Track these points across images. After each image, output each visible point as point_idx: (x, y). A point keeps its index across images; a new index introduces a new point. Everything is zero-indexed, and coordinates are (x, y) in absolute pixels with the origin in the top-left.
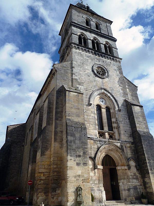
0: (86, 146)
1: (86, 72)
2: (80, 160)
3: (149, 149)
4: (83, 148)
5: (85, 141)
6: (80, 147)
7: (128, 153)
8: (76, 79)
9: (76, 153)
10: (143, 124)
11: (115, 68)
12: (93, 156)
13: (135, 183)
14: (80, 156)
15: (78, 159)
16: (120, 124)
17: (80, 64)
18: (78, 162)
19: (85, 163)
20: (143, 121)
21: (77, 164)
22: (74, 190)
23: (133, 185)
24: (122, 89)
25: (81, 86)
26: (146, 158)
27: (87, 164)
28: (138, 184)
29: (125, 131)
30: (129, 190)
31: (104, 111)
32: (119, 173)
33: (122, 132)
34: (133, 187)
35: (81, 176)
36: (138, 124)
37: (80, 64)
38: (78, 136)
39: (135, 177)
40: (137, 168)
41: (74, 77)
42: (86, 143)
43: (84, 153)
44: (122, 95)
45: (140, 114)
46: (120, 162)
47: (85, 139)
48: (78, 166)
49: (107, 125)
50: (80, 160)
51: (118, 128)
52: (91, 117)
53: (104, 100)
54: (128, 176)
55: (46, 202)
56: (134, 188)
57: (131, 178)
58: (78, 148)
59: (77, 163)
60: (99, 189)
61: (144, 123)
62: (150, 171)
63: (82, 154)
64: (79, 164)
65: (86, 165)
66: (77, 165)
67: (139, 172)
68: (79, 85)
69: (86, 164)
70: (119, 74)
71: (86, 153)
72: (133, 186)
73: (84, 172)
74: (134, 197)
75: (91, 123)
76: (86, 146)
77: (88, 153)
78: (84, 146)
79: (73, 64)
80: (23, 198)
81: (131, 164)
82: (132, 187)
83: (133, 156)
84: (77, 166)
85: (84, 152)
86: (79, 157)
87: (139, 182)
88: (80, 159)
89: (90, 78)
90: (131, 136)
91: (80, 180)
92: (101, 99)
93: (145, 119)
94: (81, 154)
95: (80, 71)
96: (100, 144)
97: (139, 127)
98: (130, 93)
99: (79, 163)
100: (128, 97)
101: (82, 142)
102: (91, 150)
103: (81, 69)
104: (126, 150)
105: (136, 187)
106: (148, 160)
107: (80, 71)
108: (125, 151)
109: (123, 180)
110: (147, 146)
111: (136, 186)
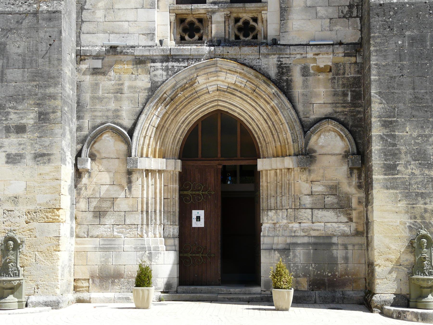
0: (51, 90)
2: (20, 144)
3: (405, 72)
4: (40, 95)
5: (47, 69)
6: (26, 94)
7: (314, 100)
9: (6, 120)
12: (127, 122)
13: (330, 223)
14: (21, 129)
15: (14, 139)
18: (14, 151)
19: (43, 155)
21: (8, 158)
23: (313, 233)
26: (373, 120)
27: (52, 157)
28: (345, 228)
30: (285, 251)
32: (266, 184)
34: (312, 240)
35: (20, 200)
38: (20, 51)
39: (330, 200)
40: (348, 164)
42: (53, 78)
43: (39, 117)
46: (270, 138)
47: (50, 61)
48: (10, 166)
50: (20, 144)
54: (297, 198)
55: (419, 317)
56: (315, 244)
57: (308, 206)
58: (17, 98)
59: (8, 154)
60: (140, 242)
62: (382, 177)
63: (32, 122)
64: (15, 159)
65: (49, 160)
66: (7, 162)
67: (359, 177)
69: (46, 158)
71: (52, 116)
72: (309, 236)
73: (37, 185)
74: (305, 276)
76: (51, 90)
77: (59, 114)
78: (42, 91)
81: (322, 147)
82: (306, 240)
83: (339, 110)
84: (7, 165)
85: (40, 114)
86: (17, 133)
87: (351, 220)
88: (25, 138)
90: (350, 11)
91: (16, 211)
94: (30, 119)
96: (167, 69)
99: (17, 155)
101: (37, 75)
102: (117, 99)
104: (305, 85)
105: (326, 241)
106: (386, 124)
108: (298, 90)
109: (274, 211)
110: (400, 56)
111: (330, 237)
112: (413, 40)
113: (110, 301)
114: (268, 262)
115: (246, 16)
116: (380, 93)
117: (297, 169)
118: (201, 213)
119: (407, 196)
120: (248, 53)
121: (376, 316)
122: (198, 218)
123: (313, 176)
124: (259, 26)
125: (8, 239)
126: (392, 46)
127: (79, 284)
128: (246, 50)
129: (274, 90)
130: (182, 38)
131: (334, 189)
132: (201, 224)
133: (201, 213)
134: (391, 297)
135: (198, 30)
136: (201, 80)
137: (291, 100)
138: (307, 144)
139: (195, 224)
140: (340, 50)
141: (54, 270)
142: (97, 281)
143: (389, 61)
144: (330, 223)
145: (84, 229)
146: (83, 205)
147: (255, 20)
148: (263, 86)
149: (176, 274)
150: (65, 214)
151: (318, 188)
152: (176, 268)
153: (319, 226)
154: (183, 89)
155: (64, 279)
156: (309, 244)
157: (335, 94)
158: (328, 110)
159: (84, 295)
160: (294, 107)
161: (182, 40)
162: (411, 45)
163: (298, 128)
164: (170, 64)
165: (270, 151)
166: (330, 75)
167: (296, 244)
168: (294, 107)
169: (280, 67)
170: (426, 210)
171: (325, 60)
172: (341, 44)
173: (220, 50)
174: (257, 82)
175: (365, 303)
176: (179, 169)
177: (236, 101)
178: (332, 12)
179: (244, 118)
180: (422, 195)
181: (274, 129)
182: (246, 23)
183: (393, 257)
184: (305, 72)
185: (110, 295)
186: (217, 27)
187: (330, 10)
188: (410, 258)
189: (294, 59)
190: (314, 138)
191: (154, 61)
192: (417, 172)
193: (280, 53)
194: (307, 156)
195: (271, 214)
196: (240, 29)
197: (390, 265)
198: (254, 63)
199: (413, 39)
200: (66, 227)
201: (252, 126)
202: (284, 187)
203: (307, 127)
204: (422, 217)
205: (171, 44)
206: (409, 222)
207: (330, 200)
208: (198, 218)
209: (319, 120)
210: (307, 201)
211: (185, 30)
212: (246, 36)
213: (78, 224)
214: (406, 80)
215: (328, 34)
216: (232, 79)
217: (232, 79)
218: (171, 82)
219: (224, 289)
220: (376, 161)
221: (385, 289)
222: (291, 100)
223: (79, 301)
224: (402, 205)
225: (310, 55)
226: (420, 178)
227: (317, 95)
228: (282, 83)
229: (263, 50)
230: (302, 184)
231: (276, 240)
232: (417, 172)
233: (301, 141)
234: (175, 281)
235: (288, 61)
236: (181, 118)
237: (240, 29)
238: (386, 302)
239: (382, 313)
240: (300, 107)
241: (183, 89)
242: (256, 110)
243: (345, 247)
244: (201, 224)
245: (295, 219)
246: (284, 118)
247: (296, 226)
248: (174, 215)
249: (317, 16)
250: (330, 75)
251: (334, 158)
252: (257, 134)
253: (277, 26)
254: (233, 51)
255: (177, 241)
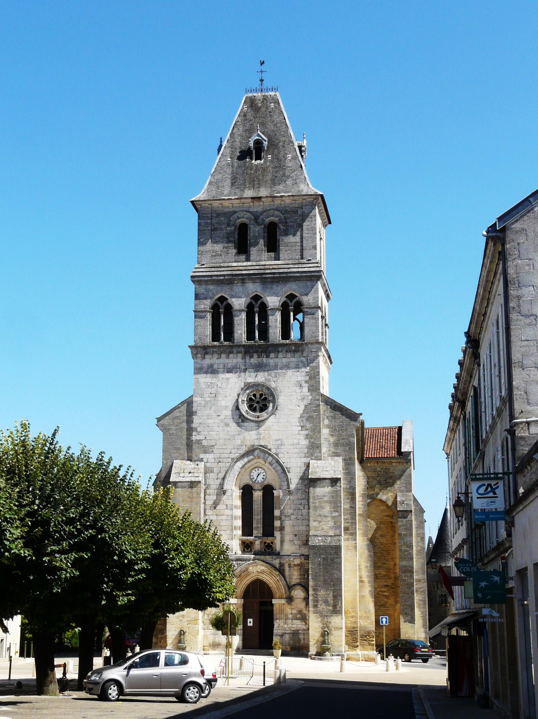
1: (221, 417)
3: (321, 570)
7: (293, 577)
8: (199, 442)
10: (329, 519)
11: (300, 379)
13: (298, 625)
16: (286, 522)
17: (209, 399)
20: (332, 514)
22: (176, 633)
24: (307, 435)
25: (208, 456)
29: (296, 535)
30: (282, 636)
31: (258, 495)
32: (276, 609)
33: (287, 538)
34: (292, 632)
36: (315, 521)
37: (209, 399)
39: (299, 616)
41: (195, 437)
44: (306, 451)
45: (326, 499)
49: (260, 526)
51: (282, 529)
52: (224, 518)
53: (263, 471)
61: (333, 518)
68: (205, 452)
70: (309, 394)
75: (223, 528)
79: (195, 405)
80: (527, 604)
82: (289, 632)
89: (228, 429)
92: (256, 469)
93: (337, 507)
95: (209, 417)
97: (316, 527)
98: (332, 440)
100: (320, 452)
103: (212, 411)
104: (290, 571)
106: (314, 590)
107: (209, 418)
108: (287, 573)
110: (319, 565)
111: (299, 630)
112: (324, 559)
113: (216, 654)
114: (276, 639)
115: (268, 541)
116: (312, 578)
117: (287, 604)
118: (251, 620)
119: (321, 616)
120: (268, 558)
121: (309, 659)
122: (250, 622)
123: (292, 607)
124: (274, 546)
125: (181, 631)
126: (317, 561)
127: (205, 648)
128: (268, 557)
129: (278, 573)
130: (244, 550)
131: (300, 612)
132: (251, 625)
133: (251, 620)
134: (314, 653)
135: (250, 547)
136: (250, 568)
137: (284, 577)
138: (290, 594)
139: (249, 624)
140: (303, 558)
141: (197, 642)
142: (212, 646)
143: (316, 566)
144: (298, 625)
145: (207, 626)
146: (206, 617)
147: (272, 543)
148: (274, 571)
149: (241, 645)
150: (200, 622)
151: (294, 611)
152: (241, 642)
153: (295, 626)
154: (244, 572)
155: (200, 646)
156: (291, 633)
157: (301, 575)
158: (298, 581)
159: (207, 652)
160: (285, 580)
161: (244, 552)
162: (323, 561)
163: (287, 588)
164: (239, 562)
165: (277, 596)
166: (299, 567)
167: (285, 633)
168: (285, 580)
169: (280, 564)
170: (327, 622)
171: (297, 561)
172: (303, 555)
173: (258, 557)
174: (272, 569)
175: (306, 656)
176: (242, 602)
177: (264, 576)
178: (299, 542)
179: (268, 582)
180: (326, 616)
181: (278, 588)
182: (269, 544)
183: (316, 638)
184: (290, 566)
185: (216, 652)
186: (258, 545)
187: (299, 542)
188: (322, 639)
189: (285, 561)
190: (293, 592)
191: (233, 561)
192: (325, 607)
193: (280, 558)
194: (290, 599)
195: (277, 621)
196: (266, 546)
197: (315, 641)
198: (271, 562)
199: (324, 558)
200: (201, 625)
201: (271, 586)
202: (282, 611)
203: (290, 588)
204: (326, 624)
205: (239, 552)
206: (321, 626)
207: (299, 616)
208: (250, 622)
209: (294, 585)
210: (290, 616)
211: (245, 547)
212: (268, 549)
213: (204, 624)
214: (321, 574)
215: (298, 551)
216: (263, 568)
217: (263, 568)
218: (239, 569)
219: (259, 650)
220: (311, 603)
221: (313, 650)
222: (284, 577)
223: (205, 654)
224: (319, 619)
225: (292, 559)
226: (326, 610)
227: (294, 575)
228: (281, 571)
229: (274, 557)
230: (288, 610)
231: (279, 631)
232: (325, 607)
233: (288, 593)
234: (241, 647)
235: (283, 562)
236: (243, 582)
237: (266, 546)
238: (313, 655)
239: (311, 659)
240: (288, 580)
241: (244, 572)
242: (271, 580)
243: (304, 634)
244: (251, 625)
245: (286, 623)
246: (282, 583)
247: (286, 626)
248: (314, 497)
249: (294, 544)
250: (299, 567)
251: (300, 600)
252: (273, 589)
253: (280, 547)
254: (262, 557)
255: (425, 585)
